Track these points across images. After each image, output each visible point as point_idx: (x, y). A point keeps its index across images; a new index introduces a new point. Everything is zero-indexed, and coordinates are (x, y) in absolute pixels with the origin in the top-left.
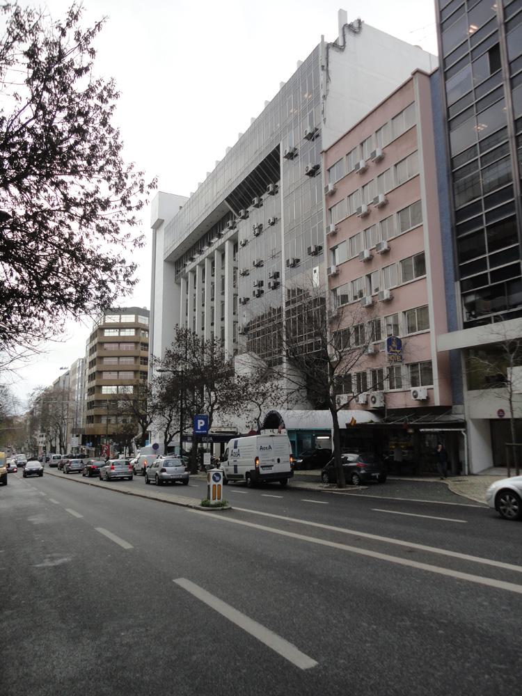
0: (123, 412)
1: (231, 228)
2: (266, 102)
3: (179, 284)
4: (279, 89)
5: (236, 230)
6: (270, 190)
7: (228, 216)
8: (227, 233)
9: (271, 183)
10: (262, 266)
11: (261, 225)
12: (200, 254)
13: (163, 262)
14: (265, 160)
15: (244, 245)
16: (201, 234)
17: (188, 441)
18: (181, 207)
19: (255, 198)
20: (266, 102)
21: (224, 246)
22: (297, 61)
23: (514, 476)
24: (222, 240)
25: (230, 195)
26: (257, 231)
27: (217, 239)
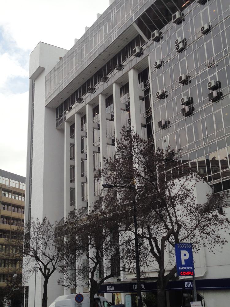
0: (168, 229)
1: (139, 55)
2: (98, 14)
3: (62, 131)
4: (84, 32)
5: (142, 57)
6: (156, 36)
7: (138, 40)
8: (131, 62)
9: (156, 29)
10: (167, 96)
11: (185, 39)
12: (80, 102)
13: (44, 107)
14: (152, 5)
15: (159, 67)
16: (82, 82)
17: (107, 292)
18: (61, 58)
19: (156, 31)
20: (98, 14)
21: (86, 107)
22: (75, 39)
23: (196, 301)
24: (84, 104)
25: (143, 16)
26: (181, 46)
27: (116, 71)
